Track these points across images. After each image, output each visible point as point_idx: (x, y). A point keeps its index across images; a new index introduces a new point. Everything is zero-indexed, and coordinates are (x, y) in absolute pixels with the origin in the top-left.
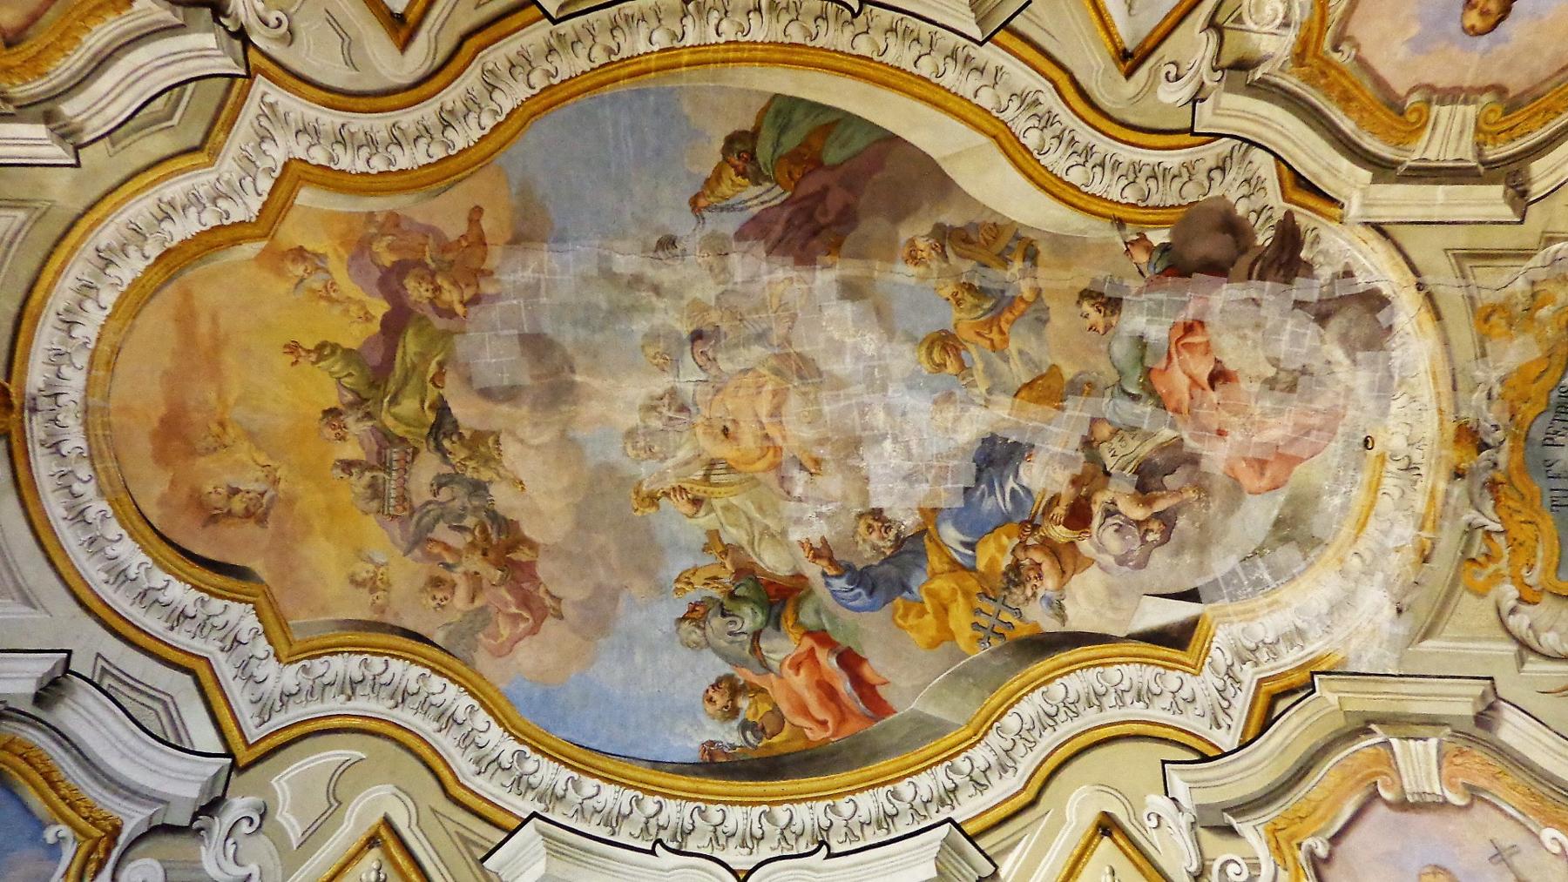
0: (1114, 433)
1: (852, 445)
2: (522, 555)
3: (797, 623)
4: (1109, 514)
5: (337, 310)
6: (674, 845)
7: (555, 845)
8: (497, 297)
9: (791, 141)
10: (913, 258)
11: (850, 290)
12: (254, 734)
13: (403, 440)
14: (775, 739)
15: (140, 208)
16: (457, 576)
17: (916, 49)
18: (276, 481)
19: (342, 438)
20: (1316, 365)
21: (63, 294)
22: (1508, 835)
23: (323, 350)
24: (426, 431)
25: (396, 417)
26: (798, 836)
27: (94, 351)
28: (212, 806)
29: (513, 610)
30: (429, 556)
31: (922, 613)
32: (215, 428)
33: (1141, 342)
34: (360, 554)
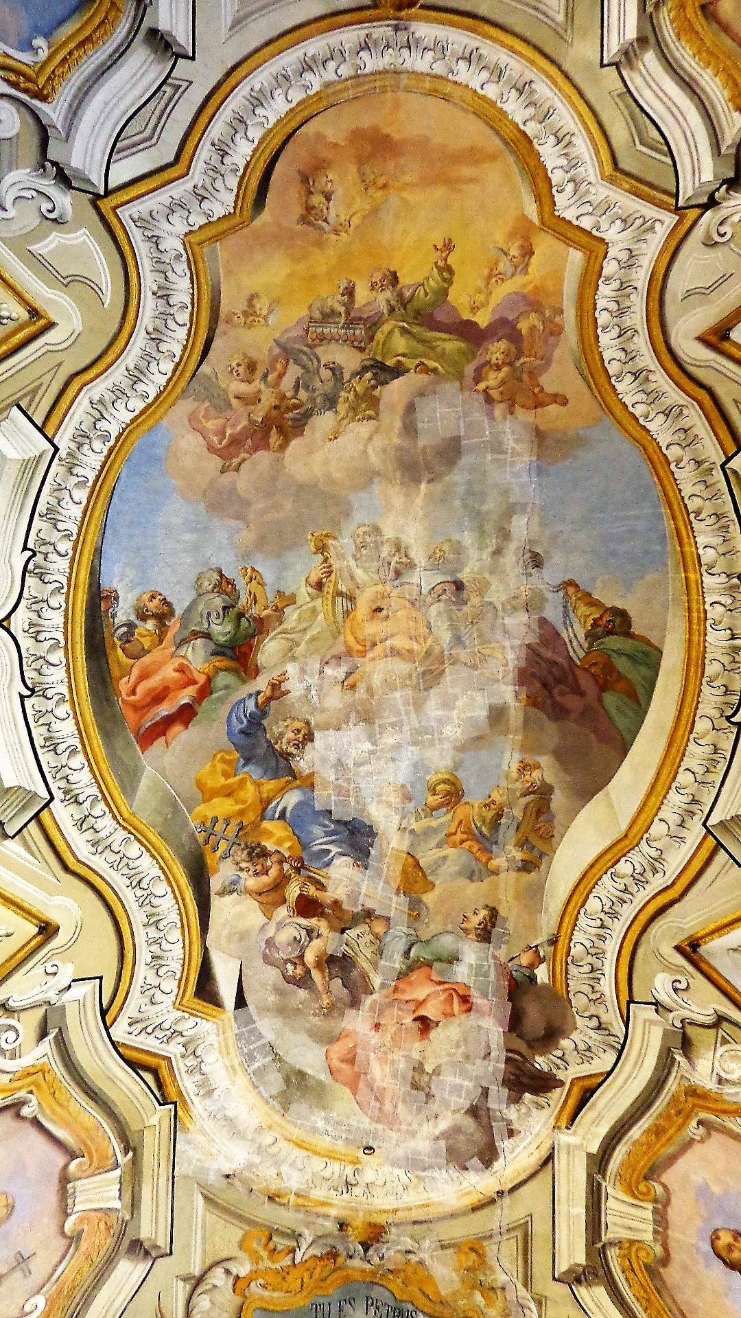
0: (377, 936)
1: (367, 717)
2: (274, 439)
3: (218, 670)
4: (310, 932)
5: (480, 283)
6: (31, 566)
7: (31, 466)
8: (491, 418)
9: (622, 664)
10: (524, 768)
11: (497, 715)
12: (124, 213)
13: (372, 339)
14: (120, 651)
15: (566, 118)
16: (258, 384)
17: (700, 770)
18: (337, 232)
19: (373, 288)
20: (434, 1106)
21: (494, 53)
22: (40, 1268)
23: (447, 272)
24: (379, 358)
25: (390, 333)
26: (38, 671)
27: (446, 79)
28: (64, 178)
29: (229, 432)
30: (274, 360)
31: (226, 775)
32: (381, 181)
33: (454, 959)
34: (276, 302)
